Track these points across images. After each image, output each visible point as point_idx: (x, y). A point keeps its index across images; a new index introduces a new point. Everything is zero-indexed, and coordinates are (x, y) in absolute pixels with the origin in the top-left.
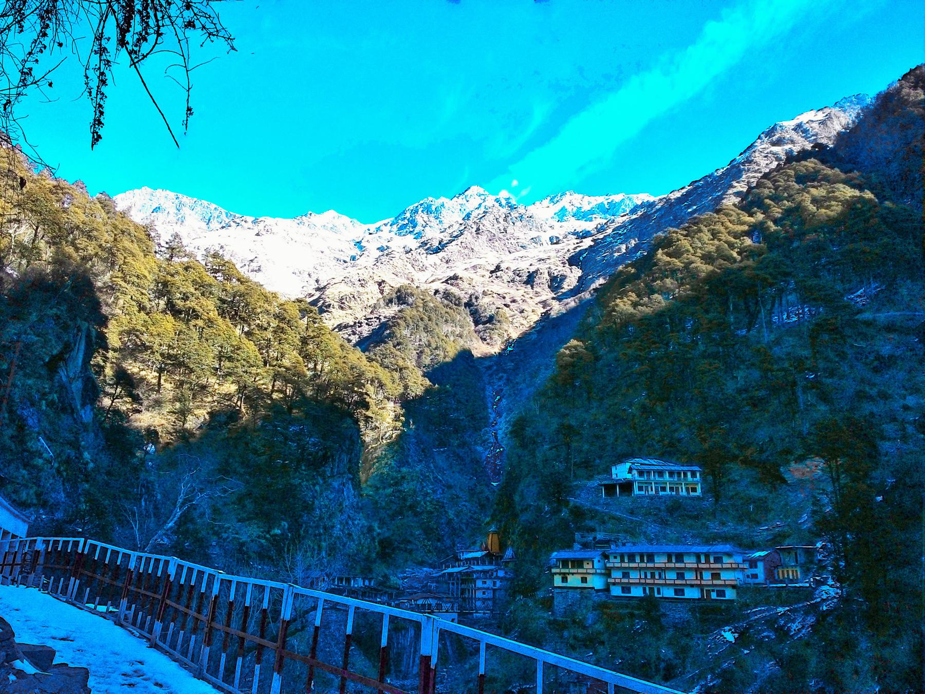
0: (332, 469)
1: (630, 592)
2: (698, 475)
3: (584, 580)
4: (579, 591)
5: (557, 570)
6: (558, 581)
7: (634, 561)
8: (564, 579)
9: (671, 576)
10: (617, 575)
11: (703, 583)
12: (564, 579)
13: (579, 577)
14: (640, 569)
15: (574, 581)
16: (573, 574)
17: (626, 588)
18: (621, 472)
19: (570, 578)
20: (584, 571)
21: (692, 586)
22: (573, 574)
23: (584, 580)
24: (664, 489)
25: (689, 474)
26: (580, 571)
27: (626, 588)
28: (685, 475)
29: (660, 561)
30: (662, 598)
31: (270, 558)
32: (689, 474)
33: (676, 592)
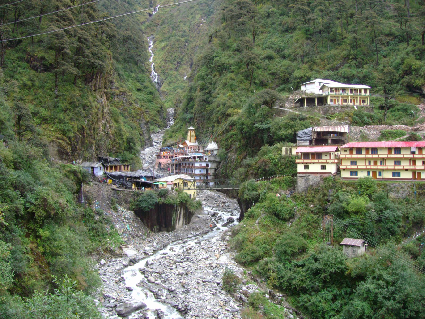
0: (96, 84)
1: (399, 176)
2: (368, 91)
3: (323, 167)
4: (319, 175)
5: (301, 161)
6: (300, 168)
7: (361, 153)
8: (306, 167)
9: (390, 165)
10: (346, 165)
11: (417, 168)
12: (306, 167)
13: (319, 166)
14: (365, 159)
15: (315, 168)
16: (314, 163)
17: (354, 172)
18: (312, 89)
19: (311, 166)
20: (324, 161)
21: (407, 170)
22: (314, 163)
23: (323, 167)
24: (345, 101)
25: (363, 91)
26: (320, 161)
27: (396, 173)
28: (360, 91)
29: (382, 154)
30: (383, 178)
31: (67, 154)
32: (363, 91)
33: (394, 174)
